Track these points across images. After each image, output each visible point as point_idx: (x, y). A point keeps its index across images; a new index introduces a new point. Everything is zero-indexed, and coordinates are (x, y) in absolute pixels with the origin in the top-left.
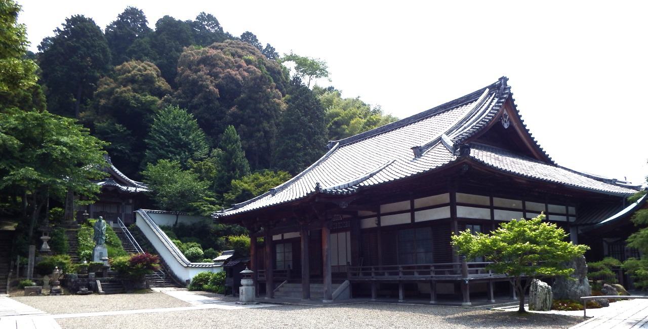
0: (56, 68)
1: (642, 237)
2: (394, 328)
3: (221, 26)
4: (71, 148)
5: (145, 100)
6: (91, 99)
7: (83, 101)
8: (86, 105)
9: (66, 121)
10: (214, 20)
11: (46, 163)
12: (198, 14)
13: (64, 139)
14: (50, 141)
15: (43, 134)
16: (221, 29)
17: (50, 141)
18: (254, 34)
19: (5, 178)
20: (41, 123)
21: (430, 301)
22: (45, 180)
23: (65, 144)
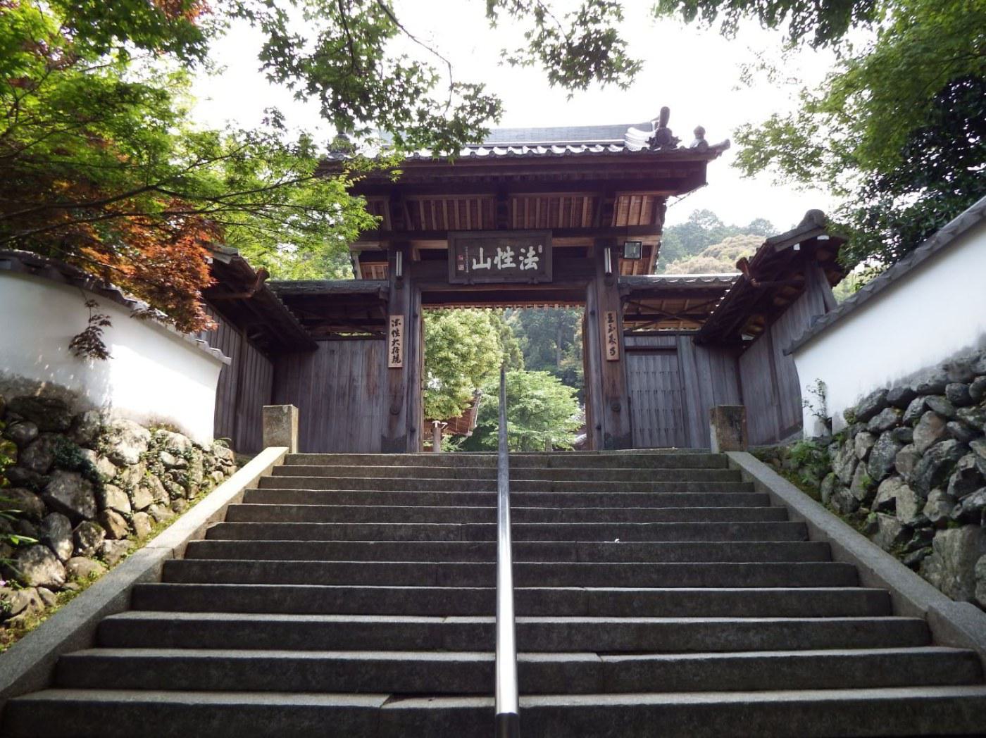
0: (535, 317)
1: (148, 250)
2: (275, 1)
3: (720, 220)
4: (544, 400)
5: (102, 92)
6: (572, 342)
7: (564, 347)
8: (567, 351)
9: (539, 375)
10: (711, 214)
11: (524, 417)
12: (691, 213)
13: (537, 393)
14: (526, 396)
15: (520, 391)
16: (721, 223)
17: (526, 396)
18: (766, 219)
19: (492, 434)
20: (518, 381)
21: (721, 426)
22: (523, 432)
23: (538, 398)
